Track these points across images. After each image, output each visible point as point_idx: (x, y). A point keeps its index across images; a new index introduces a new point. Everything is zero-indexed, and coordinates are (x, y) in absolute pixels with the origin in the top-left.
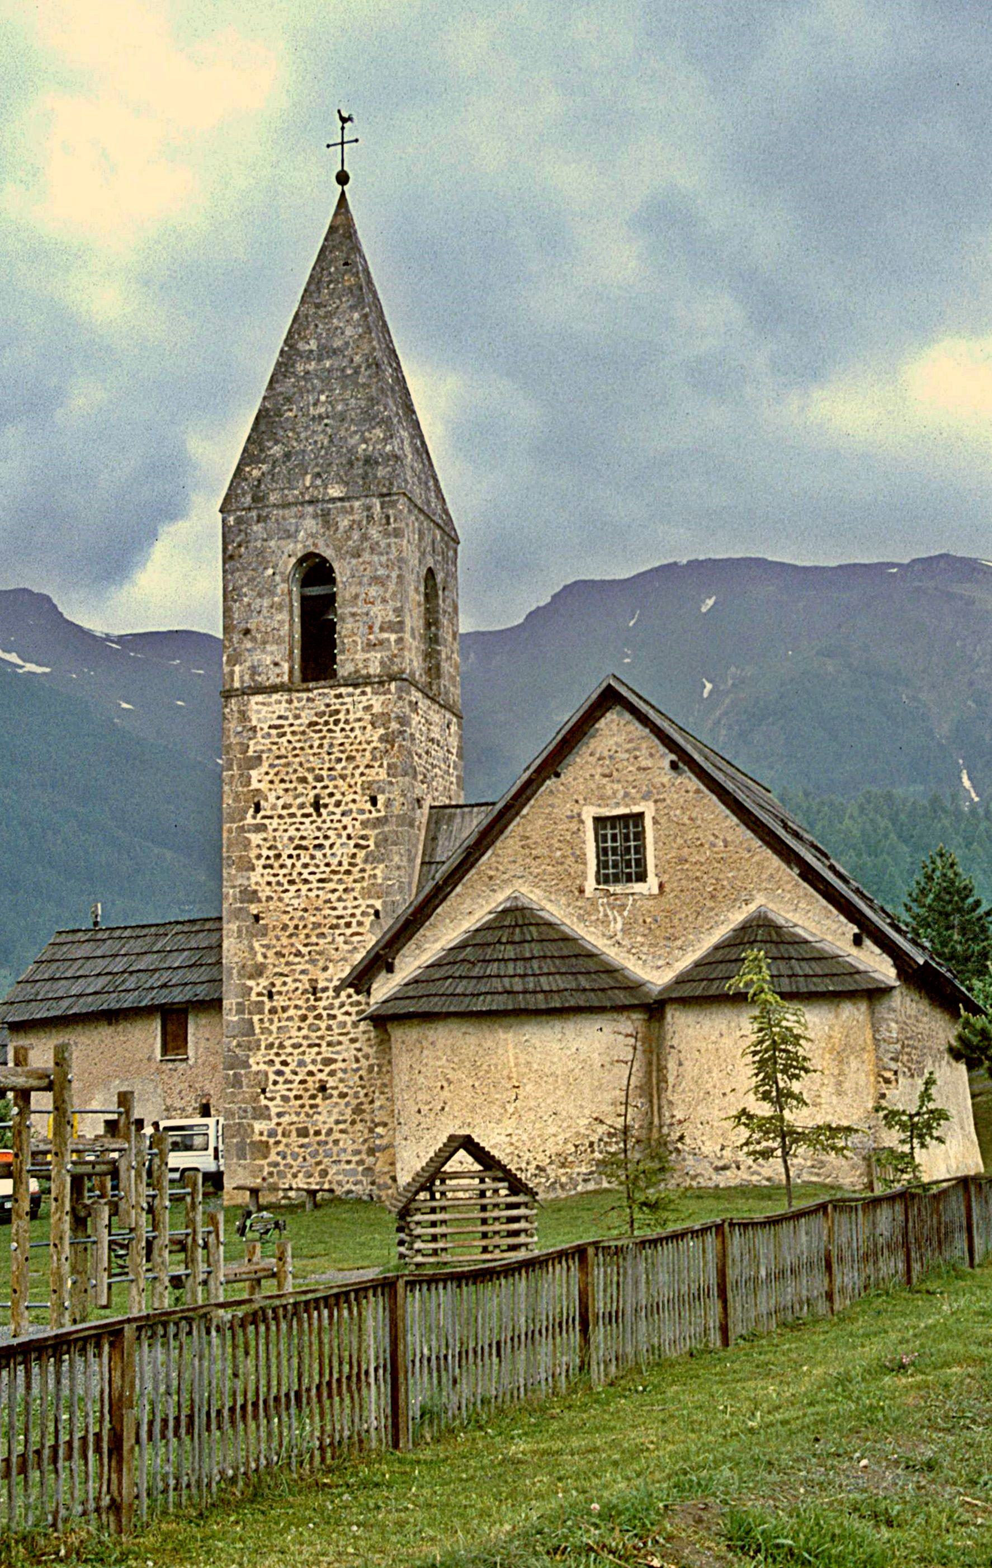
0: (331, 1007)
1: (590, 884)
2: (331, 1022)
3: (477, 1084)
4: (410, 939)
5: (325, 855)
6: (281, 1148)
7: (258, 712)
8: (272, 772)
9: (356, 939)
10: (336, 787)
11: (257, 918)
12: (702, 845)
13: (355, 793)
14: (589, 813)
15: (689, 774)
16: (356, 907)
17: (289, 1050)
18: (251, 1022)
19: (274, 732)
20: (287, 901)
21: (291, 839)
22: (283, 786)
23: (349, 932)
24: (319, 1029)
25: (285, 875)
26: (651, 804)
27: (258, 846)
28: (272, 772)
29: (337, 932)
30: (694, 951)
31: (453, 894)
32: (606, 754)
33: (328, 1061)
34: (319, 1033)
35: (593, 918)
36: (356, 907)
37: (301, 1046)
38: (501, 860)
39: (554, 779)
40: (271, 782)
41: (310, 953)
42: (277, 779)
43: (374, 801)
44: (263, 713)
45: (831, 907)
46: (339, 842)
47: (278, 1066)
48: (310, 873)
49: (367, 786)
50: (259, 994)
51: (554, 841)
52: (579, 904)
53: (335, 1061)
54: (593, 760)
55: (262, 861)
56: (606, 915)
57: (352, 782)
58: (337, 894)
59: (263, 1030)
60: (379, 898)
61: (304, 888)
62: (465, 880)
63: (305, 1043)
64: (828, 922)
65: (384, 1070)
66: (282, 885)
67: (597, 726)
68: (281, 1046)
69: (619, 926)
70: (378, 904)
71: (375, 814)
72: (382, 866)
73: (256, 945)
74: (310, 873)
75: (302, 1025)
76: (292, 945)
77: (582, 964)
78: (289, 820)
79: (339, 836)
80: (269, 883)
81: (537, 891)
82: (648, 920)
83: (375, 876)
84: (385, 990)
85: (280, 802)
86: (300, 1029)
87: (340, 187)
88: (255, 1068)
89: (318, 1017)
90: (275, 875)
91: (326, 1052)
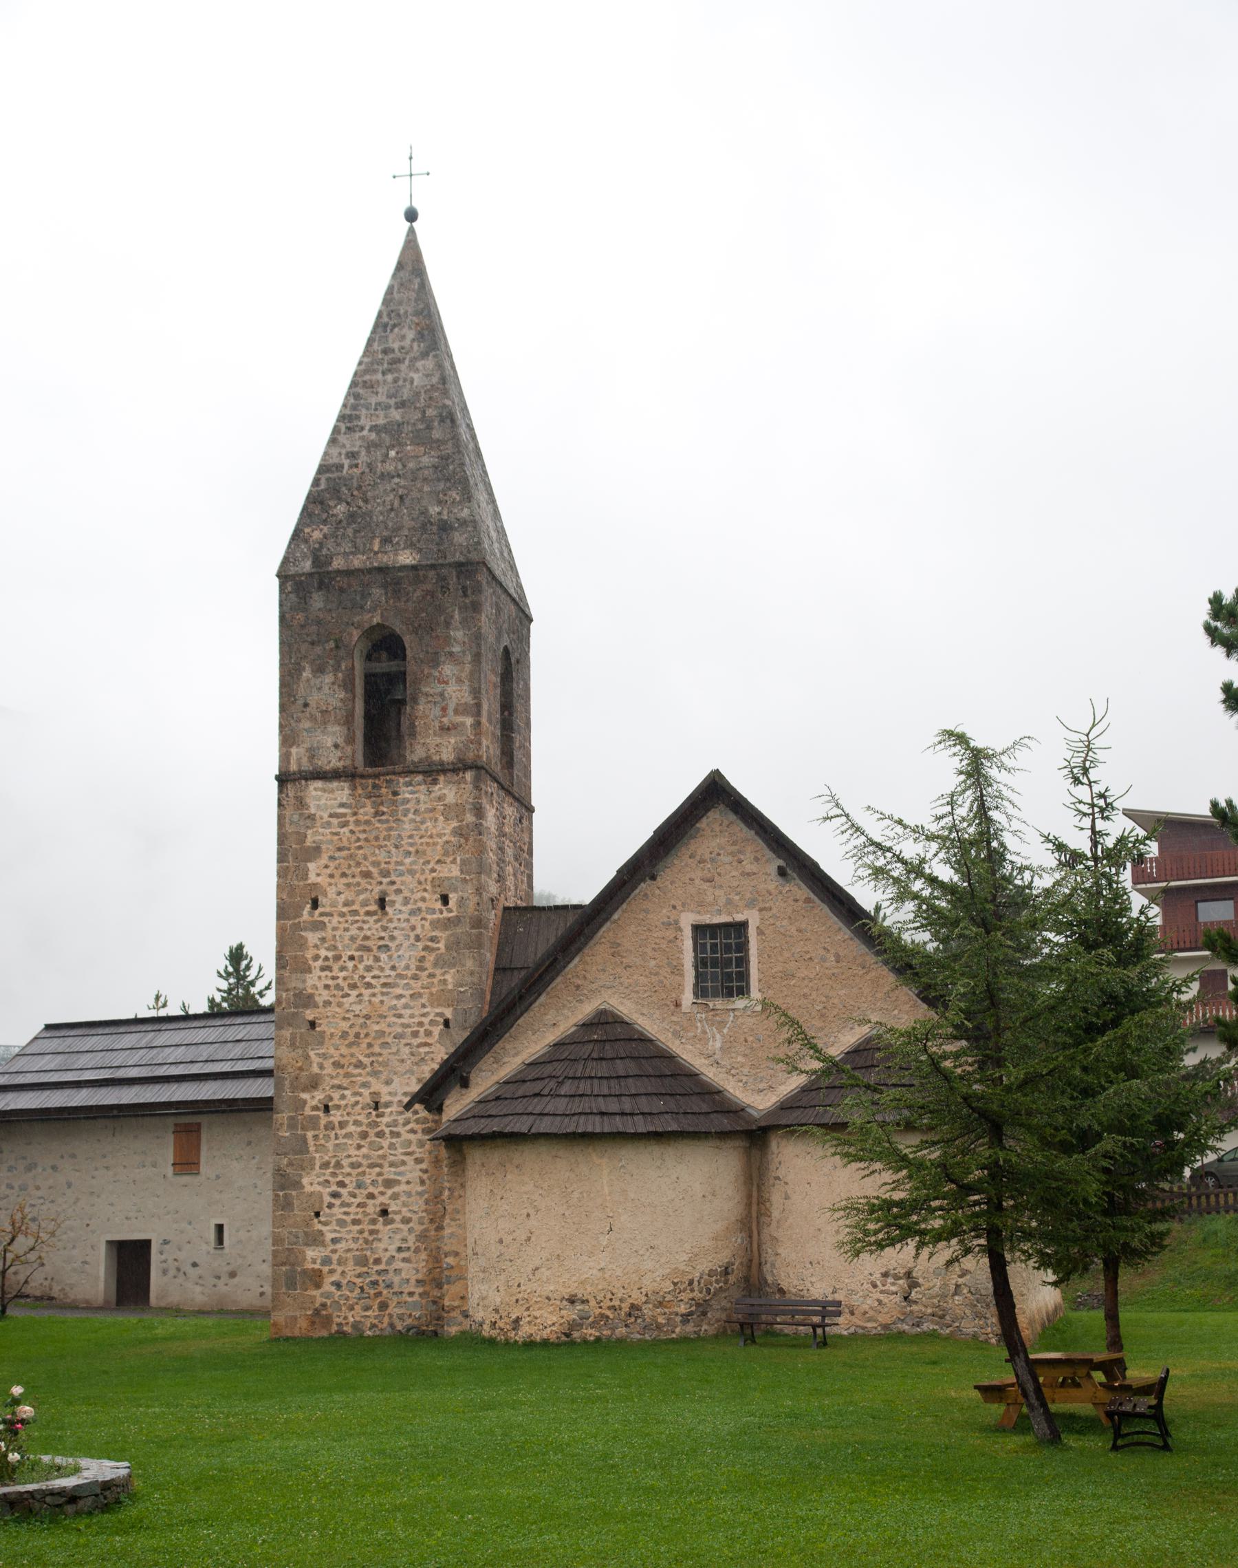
1: (688, 997)
2: (394, 1140)
3: (567, 1214)
5: (390, 957)
9: (423, 1050)
10: (403, 883)
11: (313, 1025)
13: (425, 890)
14: (688, 920)
16: (423, 1015)
17: (348, 1170)
19: (335, 821)
20: (347, 1006)
21: (353, 939)
22: (344, 880)
23: (415, 1042)
24: (382, 1148)
25: (345, 979)
27: (316, 946)
28: (332, 865)
31: (537, 1003)
32: (707, 856)
33: (389, 1183)
34: (380, 1152)
36: (423, 1015)
37: (360, 1165)
39: (649, 882)
40: (331, 876)
42: (337, 873)
43: (445, 899)
44: (323, 801)
47: (334, 1188)
48: (374, 977)
50: (315, 1108)
52: (674, 1018)
53: (398, 1182)
55: (320, 963)
56: (704, 1032)
57: (422, 879)
58: (403, 1001)
61: (367, 993)
63: (365, 1162)
65: (456, 1194)
67: (698, 825)
68: (338, 1165)
69: (718, 1045)
70: (448, 1013)
71: (445, 914)
72: (452, 971)
73: (312, 1054)
74: (374, 977)
76: (352, 1055)
78: (350, 919)
80: (327, 987)
81: (628, 1003)
82: (750, 1039)
86: (359, 1147)
87: (409, 224)
88: (308, 1189)
90: (333, 978)
91: (389, 1173)
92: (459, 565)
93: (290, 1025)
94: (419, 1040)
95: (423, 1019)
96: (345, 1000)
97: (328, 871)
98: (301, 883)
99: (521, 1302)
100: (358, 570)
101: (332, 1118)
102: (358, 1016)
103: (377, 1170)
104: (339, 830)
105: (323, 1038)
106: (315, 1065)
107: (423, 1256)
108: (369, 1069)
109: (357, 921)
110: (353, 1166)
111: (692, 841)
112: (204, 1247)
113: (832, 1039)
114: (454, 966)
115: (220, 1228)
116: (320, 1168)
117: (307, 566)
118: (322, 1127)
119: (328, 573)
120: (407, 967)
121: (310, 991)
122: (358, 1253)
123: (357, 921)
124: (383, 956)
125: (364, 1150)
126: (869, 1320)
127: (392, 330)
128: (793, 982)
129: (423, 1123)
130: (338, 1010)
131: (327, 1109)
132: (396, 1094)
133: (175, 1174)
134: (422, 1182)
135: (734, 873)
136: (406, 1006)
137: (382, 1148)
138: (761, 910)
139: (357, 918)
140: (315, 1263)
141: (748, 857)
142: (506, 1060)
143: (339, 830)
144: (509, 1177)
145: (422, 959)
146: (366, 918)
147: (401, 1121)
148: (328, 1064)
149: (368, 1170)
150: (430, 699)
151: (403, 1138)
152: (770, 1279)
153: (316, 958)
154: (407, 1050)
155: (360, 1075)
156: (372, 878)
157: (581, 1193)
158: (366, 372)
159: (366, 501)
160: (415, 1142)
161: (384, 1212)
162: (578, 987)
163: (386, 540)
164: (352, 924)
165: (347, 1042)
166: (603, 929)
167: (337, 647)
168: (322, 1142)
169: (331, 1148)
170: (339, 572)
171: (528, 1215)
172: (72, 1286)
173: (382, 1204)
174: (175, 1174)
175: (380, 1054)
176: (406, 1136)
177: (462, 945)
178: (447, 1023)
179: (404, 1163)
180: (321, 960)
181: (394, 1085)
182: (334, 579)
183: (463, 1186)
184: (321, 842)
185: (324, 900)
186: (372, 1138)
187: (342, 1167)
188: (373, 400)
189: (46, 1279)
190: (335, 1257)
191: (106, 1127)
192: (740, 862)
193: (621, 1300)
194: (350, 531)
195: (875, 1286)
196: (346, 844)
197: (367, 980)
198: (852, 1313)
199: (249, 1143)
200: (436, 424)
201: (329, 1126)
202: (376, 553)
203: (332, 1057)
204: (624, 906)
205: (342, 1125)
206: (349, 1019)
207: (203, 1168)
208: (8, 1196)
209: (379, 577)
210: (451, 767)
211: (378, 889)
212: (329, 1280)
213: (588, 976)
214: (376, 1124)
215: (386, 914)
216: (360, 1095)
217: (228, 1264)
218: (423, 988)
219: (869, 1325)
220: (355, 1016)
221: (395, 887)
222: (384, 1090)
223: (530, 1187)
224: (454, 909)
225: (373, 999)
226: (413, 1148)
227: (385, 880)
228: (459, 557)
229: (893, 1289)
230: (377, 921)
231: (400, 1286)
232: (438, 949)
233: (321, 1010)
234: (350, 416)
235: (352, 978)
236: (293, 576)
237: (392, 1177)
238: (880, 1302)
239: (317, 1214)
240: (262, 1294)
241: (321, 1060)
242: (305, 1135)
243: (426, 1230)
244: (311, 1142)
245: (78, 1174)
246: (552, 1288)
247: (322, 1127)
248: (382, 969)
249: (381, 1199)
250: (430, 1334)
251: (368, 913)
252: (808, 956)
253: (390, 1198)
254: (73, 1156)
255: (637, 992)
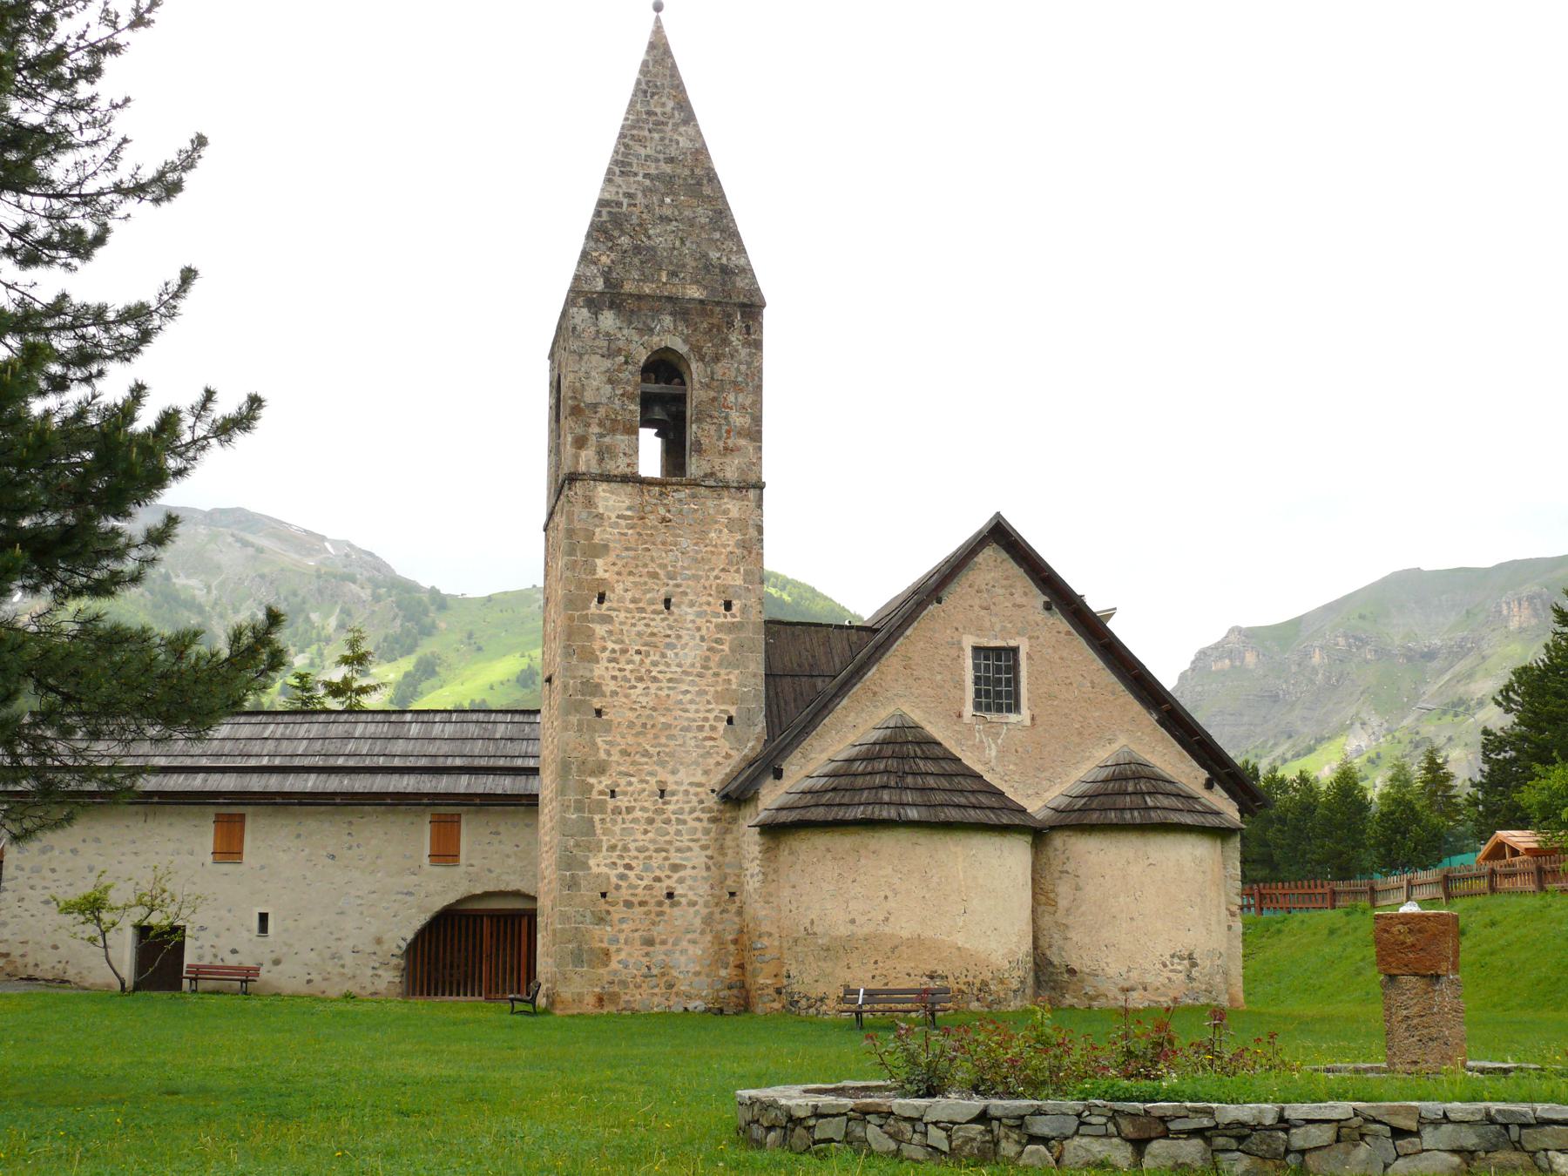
0: (681, 812)
1: (968, 709)
2: (680, 827)
3: (927, 896)
4: (797, 747)
5: (676, 654)
6: (623, 956)
7: (606, 499)
8: (620, 563)
9: (709, 743)
10: (688, 587)
11: (599, 713)
12: (1071, 683)
13: (710, 595)
14: (969, 642)
15: (1060, 616)
16: (708, 711)
17: (635, 853)
18: (591, 821)
19: (622, 522)
20: (634, 697)
21: (639, 634)
22: (631, 579)
23: (701, 735)
24: (668, 833)
25: (631, 671)
26: (1026, 640)
27: (603, 638)
28: (620, 563)
29: (690, 735)
30: (1061, 783)
31: (839, 706)
32: (984, 587)
33: (675, 868)
34: (667, 838)
35: (970, 743)
36: (708, 711)
37: (647, 850)
38: (883, 677)
39: (936, 605)
40: (619, 574)
41: (659, 753)
42: (625, 571)
43: (728, 606)
44: (611, 502)
45: (1185, 753)
46: (692, 644)
47: (621, 870)
48: (660, 672)
49: (722, 589)
50: (601, 793)
51: (935, 665)
52: (956, 728)
53: (685, 867)
54: (972, 591)
55: (607, 654)
56: (981, 742)
57: (707, 584)
58: (689, 696)
59: (606, 832)
60: (733, 704)
61: (653, 686)
62: (850, 693)
63: (652, 847)
64: (1182, 765)
65: (769, 878)
66: (629, 681)
67: (975, 559)
68: (626, 849)
69: (994, 753)
70: (733, 711)
71: (729, 619)
72: (737, 672)
73: (599, 740)
74: (660, 672)
75: (649, 828)
76: (639, 744)
77: (967, 784)
78: (638, 615)
79: (693, 638)
80: (614, 678)
81: (917, 711)
82: (1020, 750)
83: (729, 681)
84: (773, 797)
85: (629, 595)
86: (646, 832)
87: (655, 14)
88: (595, 870)
89: (667, 821)
90: (620, 670)
91: (676, 858)
92: (743, 305)
93: (577, 711)
94: (705, 734)
95: (708, 715)
96: (632, 691)
97: (616, 569)
98: (589, 577)
99: (877, 978)
100: (647, 295)
101: (619, 803)
102: (645, 707)
103: (664, 854)
104: (626, 531)
105: (611, 726)
106: (602, 751)
107: (709, 937)
108: (655, 758)
109: (645, 618)
110: (639, 850)
111: (971, 573)
112: (245, 935)
113: (1088, 754)
114: (738, 667)
115: (263, 918)
116: (607, 850)
117: (600, 285)
118: (609, 811)
119: (619, 294)
120: (693, 665)
121: (597, 680)
122: (645, 933)
123: (645, 618)
124: (670, 653)
125: (650, 835)
126: (1161, 995)
127: (651, 97)
128: (1055, 703)
129: (709, 812)
130: (624, 700)
131: (613, 794)
132: (682, 784)
133: (215, 862)
134: (708, 868)
135: (1007, 604)
136: (691, 702)
137: (668, 833)
138: (1030, 638)
139: (644, 615)
140: (602, 941)
141: (1018, 592)
142: (813, 755)
143: (626, 531)
144: (863, 861)
145: (707, 659)
146: (652, 616)
147: (687, 810)
148: (615, 752)
149: (654, 854)
150: (715, 421)
151: (688, 826)
152: (1056, 961)
153: (604, 649)
154: (693, 743)
155: (646, 763)
156: (658, 579)
157: (940, 878)
158: (633, 127)
159: (649, 238)
160: (700, 829)
161: (670, 895)
162: (875, 694)
163: (673, 274)
164: (639, 620)
165: (634, 732)
166: (898, 643)
167: (626, 362)
168: (609, 825)
169: (618, 832)
170: (631, 295)
171: (886, 897)
172: (90, 970)
173: (668, 887)
174: (215, 862)
175: (665, 746)
176: (692, 824)
177: (745, 649)
178: (730, 721)
179: (690, 849)
180: (608, 652)
181: (680, 774)
182: (625, 300)
183: (776, 871)
184: (608, 540)
185: (612, 596)
186: (659, 824)
187: (629, 850)
188: (643, 152)
189: (60, 962)
190: (622, 937)
191: (137, 813)
192: (1012, 594)
193: (974, 977)
194: (636, 261)
195: (1165, 965)
196: (633, 546)
197: (653, 674)
198: (1145, 989)
199: (299, 836)
200: (705, 182)
201: (617, 811)
202: (665, 284)
203: (619, 745)
204: (915, 624)
205: (629, 810)
206: (636, 709)
207: (245, 858)
208: (17, 878)
209: (669, 306)
210: (735, 485)
211: (663, 590)
212: (614, 959)
213: (883, 684)
214: (663, 812)
215: (671, 614)
216: (647, 782)
217: (272, 951)
218: (708, 686)
219: (1162, 999)
220: (642, 707)
221: (680, 590)
222: (670, 779)
223: (889, 870)
224: (738, 615)
225: (659, 692)
226: (699, 835)
227: (671, 582)
228: (742, 299)
229: (1180, 968)
230: (663, 620)
231: (686, 966)
232: (723, 650)
233: (609, 699)
234: (622, 162)
235: (638, 671)
236: (587, 293)
237: (678, 861)
238: (1169, 979)
239: (604, 895)
240: (309, 981)
241: (608, 747)
242: (592, 818)
243: (712, 913)
244: (598, 825)
245: (102, 858)
246: (913, 965)
247: (609, 811)
248: (668, 665)
249: (667, 882)
250: (716, 1011)
251: (654, 612)
252: (1069, 681)
253: (676, 882)
254: (97, 840)
255: (926, 702)
